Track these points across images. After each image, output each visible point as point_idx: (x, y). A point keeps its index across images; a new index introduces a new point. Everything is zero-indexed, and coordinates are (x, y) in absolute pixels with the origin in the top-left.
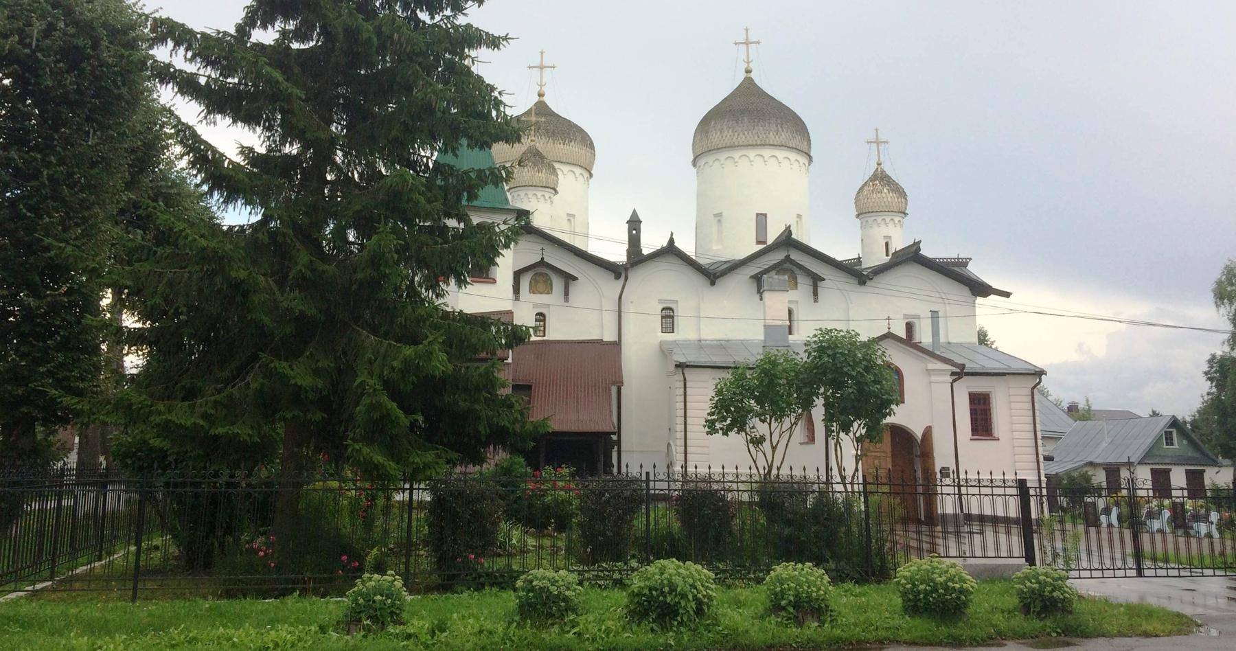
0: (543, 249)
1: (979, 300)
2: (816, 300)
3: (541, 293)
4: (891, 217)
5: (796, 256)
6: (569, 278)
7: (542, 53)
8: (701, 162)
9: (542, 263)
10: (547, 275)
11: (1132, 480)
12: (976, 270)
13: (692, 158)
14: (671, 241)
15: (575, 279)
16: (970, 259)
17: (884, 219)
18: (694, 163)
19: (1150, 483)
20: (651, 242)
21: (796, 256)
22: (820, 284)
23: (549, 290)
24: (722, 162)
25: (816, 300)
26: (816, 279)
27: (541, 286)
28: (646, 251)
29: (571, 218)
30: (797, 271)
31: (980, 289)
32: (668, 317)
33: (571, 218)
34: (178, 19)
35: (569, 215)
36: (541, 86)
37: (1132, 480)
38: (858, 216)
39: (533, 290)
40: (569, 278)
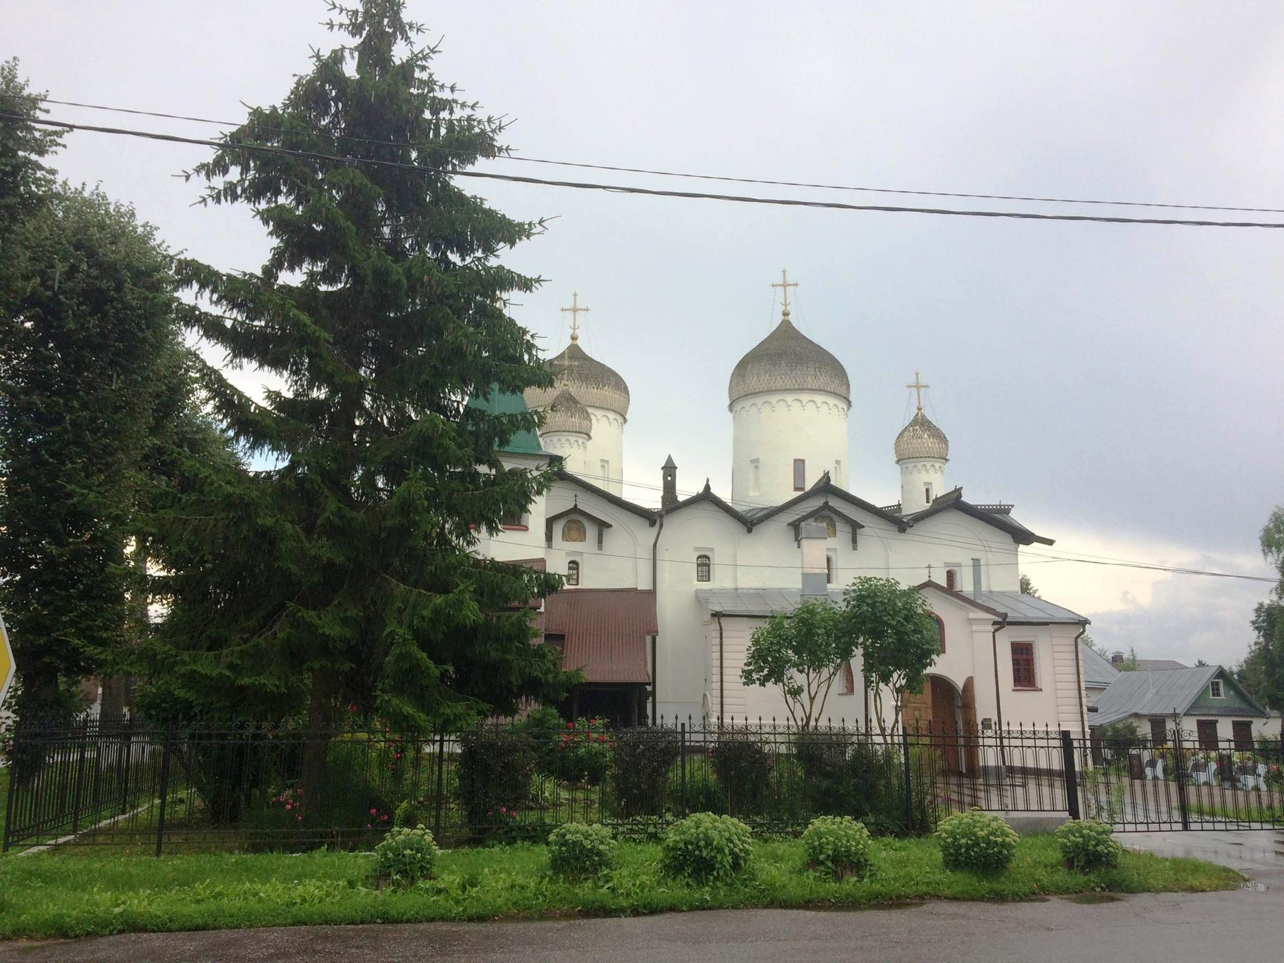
0: (576, 496)
1: (1022, 548)
2: (855, 548)
3: (574, 541)
4: (922, 464)
5: (835, 503)
6: (602, 525)
8: (738, 407)
9: (575, 510)
10: (580, 522)
11: (1178, 731)
12: (1019, 517)
13: (728, 402)
14: (707, 488)
15: (609, 526)
16: (1013, 506)
17: (924, 465)
18: (731, 408)
19: (1197, 734)
20: (686, 488)
21: (835, 503)
22: (859, 531)
23: (582, 537)
24: (759, 407)
25: (855, 548)
26: (855, 527)
27: (574, 534)
28: (681, 498)
29: (605, 464)
30: (835, 518)
31: (1023, 537)
33: (605, 464)
34: (204, 260)
35: (602, 461)
36: (574, 329)
37: (1178, 731)
38: (898, 462)
39: (566, 538)
40: (602, 525)
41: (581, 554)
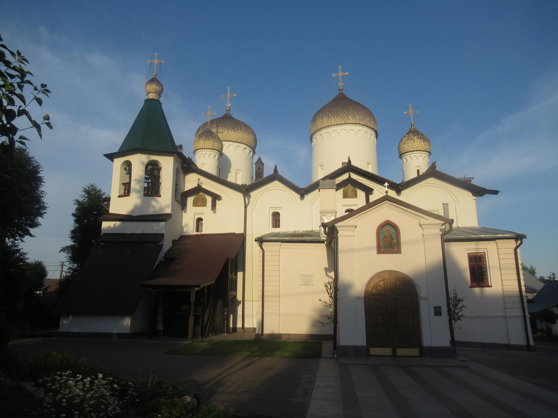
3: (200, 206)
5: (354, 176)
6: (216, 198)
7: (32, 93)
21: (354, 176)
23: (204, 204)
28: (266, 175)
32: (276, 218)
39: (195, 204)
40: (216, 198)
41: (203, 213)
